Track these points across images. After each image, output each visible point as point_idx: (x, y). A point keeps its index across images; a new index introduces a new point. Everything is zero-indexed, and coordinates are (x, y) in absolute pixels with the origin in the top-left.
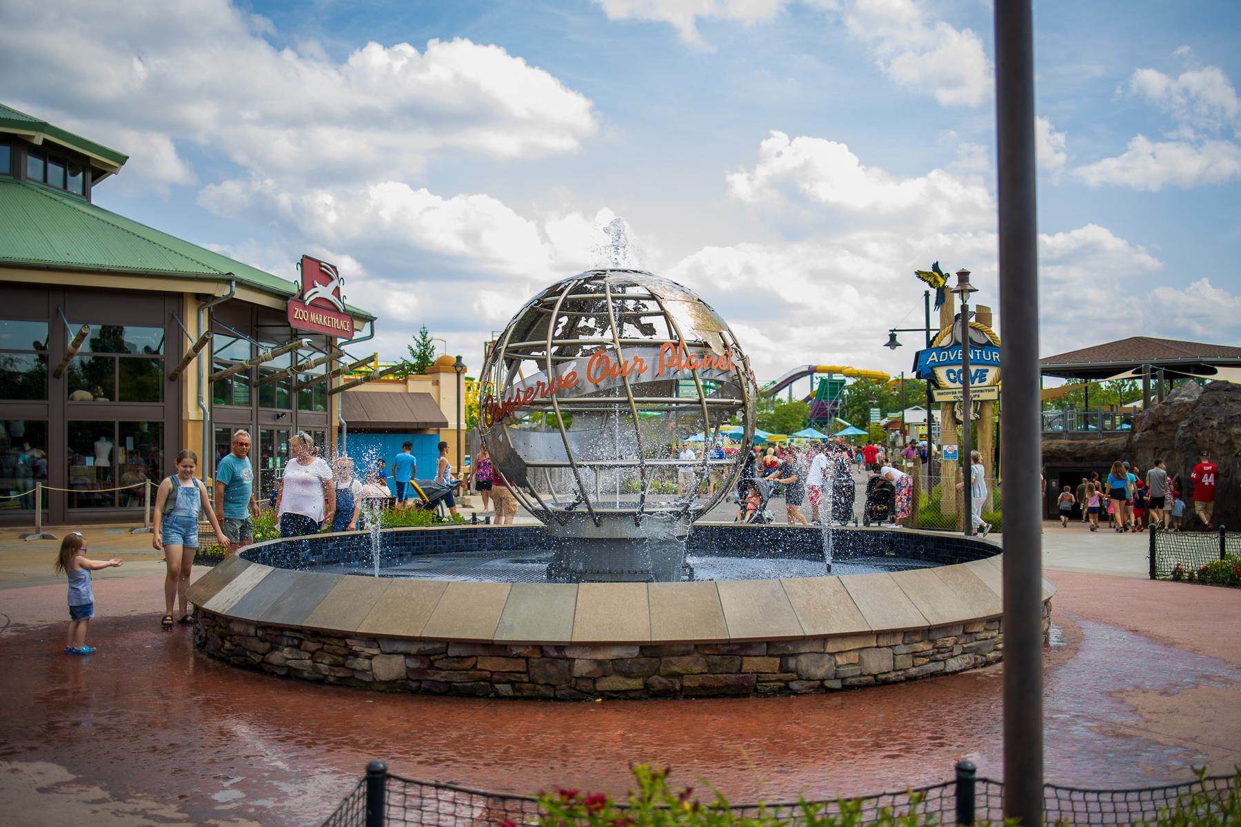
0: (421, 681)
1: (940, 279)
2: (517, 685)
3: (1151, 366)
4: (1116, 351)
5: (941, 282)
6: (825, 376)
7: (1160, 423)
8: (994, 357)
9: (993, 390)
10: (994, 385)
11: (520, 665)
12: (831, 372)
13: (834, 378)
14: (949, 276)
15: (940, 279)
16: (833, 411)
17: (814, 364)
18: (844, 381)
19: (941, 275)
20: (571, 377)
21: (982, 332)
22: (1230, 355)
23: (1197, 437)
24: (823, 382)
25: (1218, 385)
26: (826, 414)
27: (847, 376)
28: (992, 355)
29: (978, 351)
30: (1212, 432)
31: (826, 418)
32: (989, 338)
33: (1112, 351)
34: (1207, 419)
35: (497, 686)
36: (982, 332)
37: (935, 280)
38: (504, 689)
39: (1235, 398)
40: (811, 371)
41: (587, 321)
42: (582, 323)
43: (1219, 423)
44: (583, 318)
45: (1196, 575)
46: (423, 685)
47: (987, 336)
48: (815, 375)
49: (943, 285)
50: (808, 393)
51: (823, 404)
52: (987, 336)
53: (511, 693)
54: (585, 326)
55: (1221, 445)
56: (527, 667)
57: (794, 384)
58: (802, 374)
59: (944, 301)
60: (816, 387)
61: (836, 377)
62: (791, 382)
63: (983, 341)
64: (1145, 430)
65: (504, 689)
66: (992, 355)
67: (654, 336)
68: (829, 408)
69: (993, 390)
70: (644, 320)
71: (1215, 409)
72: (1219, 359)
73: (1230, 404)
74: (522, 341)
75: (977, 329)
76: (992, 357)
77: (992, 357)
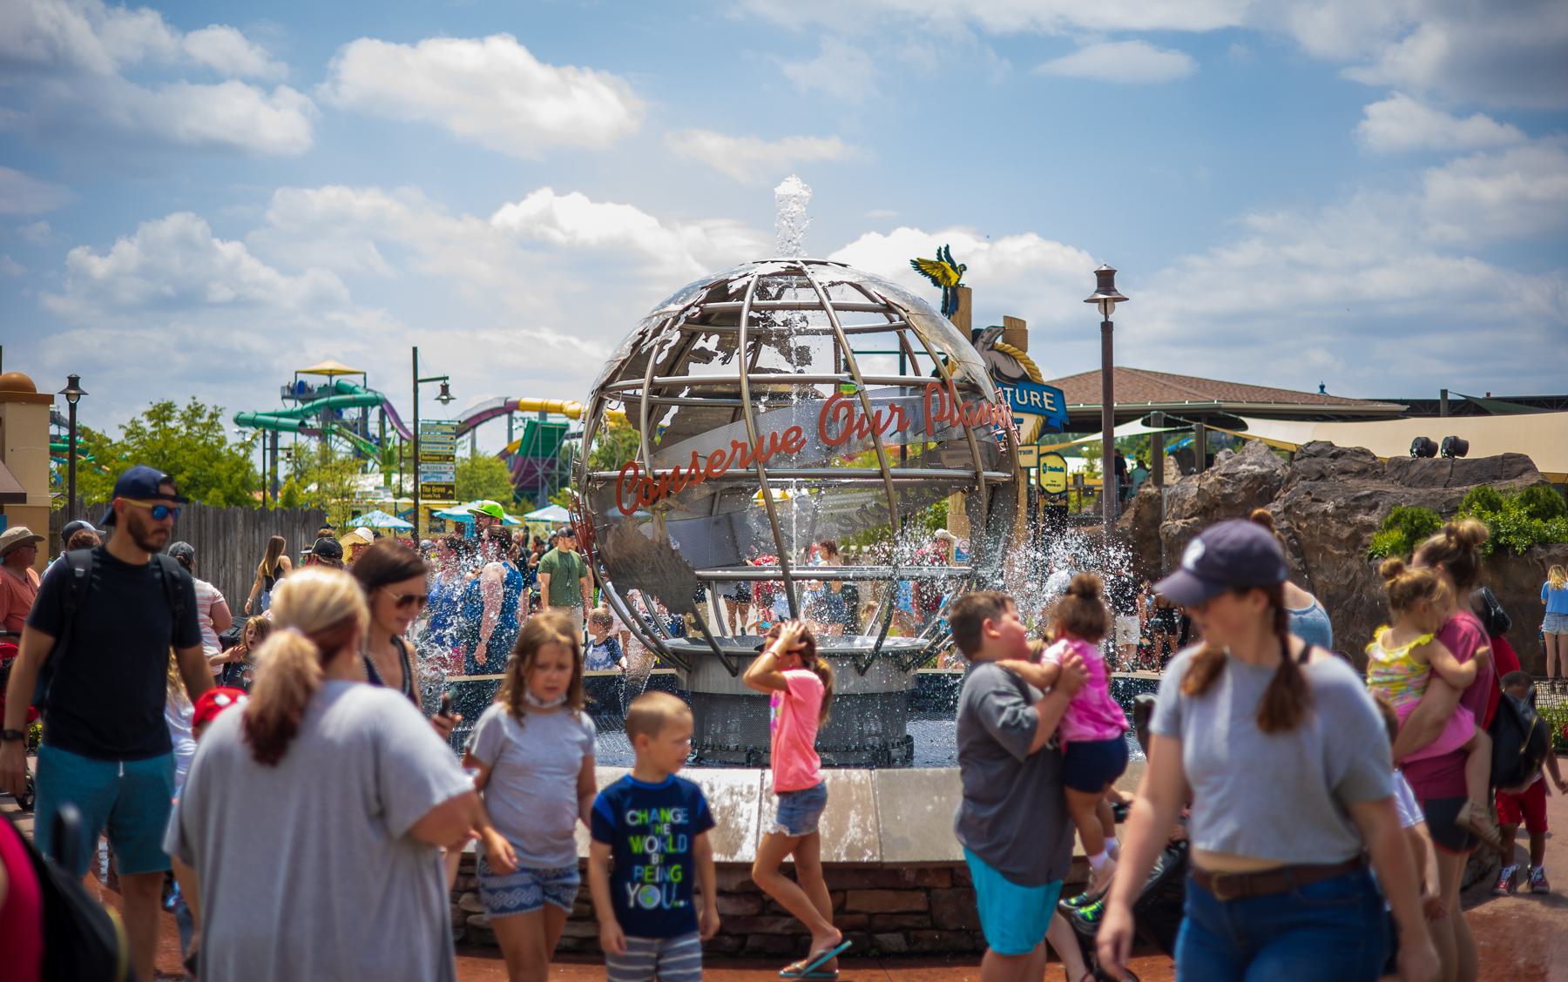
0: (745, 937)
1: (951, 273)
2: (912, 934)
3: (1164, 414)
4: (1086, 388)
5: (953, 276)
6: (534, 416)
7: (1217, 505)
8: (1032, 398)
9: (1031, 452)
10: (1032, 444)
11: (918, 902)
12: (544, 411)
13: (549, 420)
14: (965, 268)
15: (951, 273)
16: (547, 476)
17: (514, 398)
18: (567, 426)
19: (954, 267)
20: (794, 434)
21: (1015, 360)
22: (1259, 399)
23: (1299, 527)
24: (532, 427)
25: (1318, 448)
26: (536, 481)
27: (571, 418)
28: (1029, 395)
29: (1009, 390)
30: (1326, 523)
31: (537, 489)
32: (1025, 369)
33: (1079, 388)
34: (1314, 500)
35: (880, 937)
36: (1015, 360)
37: (945, 275)
38: (893, 941)
39: (1347, 468)
40: (509, 408)
41: (706, 340)
42: (700, 343)
43: (1337, 508)
44: (703, 336)
45: (595, 701)
46: (752, 942)
47: (1022, 365)
48: (517, 414)
49: (957, 283)
50: (504, 444)
51: (530, 464)
52: (1022, 365)
53: (904, 947)
54: (702, 349)
55: (1341, 541)
56: (929, 903)
57: (480, 430)
58: (493, 413)
59: (957, 309)
60: (519, 435)
61: (554, 419)
62: (474, 427)
63: (1016, 374)
64: (1191, 516)
65: (893, 941)
66: (1029, 395)
67: (806, 368)
68: (540, 471)
69: (1031, 452)
70: (796, 342)
71: (1323, 486)
72: (1245, 405)
73: (1341, 478)
74: (667, 375)
75: (1008, 354)
76: (1029, 400)
77: (1029, 400)
